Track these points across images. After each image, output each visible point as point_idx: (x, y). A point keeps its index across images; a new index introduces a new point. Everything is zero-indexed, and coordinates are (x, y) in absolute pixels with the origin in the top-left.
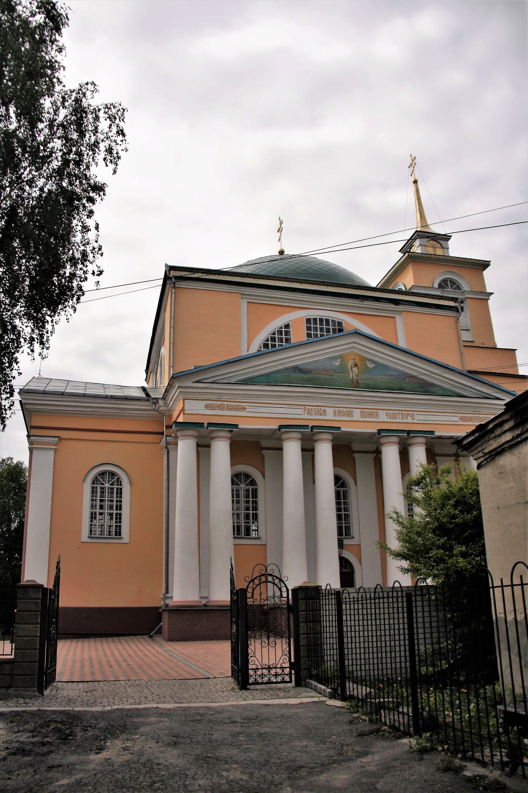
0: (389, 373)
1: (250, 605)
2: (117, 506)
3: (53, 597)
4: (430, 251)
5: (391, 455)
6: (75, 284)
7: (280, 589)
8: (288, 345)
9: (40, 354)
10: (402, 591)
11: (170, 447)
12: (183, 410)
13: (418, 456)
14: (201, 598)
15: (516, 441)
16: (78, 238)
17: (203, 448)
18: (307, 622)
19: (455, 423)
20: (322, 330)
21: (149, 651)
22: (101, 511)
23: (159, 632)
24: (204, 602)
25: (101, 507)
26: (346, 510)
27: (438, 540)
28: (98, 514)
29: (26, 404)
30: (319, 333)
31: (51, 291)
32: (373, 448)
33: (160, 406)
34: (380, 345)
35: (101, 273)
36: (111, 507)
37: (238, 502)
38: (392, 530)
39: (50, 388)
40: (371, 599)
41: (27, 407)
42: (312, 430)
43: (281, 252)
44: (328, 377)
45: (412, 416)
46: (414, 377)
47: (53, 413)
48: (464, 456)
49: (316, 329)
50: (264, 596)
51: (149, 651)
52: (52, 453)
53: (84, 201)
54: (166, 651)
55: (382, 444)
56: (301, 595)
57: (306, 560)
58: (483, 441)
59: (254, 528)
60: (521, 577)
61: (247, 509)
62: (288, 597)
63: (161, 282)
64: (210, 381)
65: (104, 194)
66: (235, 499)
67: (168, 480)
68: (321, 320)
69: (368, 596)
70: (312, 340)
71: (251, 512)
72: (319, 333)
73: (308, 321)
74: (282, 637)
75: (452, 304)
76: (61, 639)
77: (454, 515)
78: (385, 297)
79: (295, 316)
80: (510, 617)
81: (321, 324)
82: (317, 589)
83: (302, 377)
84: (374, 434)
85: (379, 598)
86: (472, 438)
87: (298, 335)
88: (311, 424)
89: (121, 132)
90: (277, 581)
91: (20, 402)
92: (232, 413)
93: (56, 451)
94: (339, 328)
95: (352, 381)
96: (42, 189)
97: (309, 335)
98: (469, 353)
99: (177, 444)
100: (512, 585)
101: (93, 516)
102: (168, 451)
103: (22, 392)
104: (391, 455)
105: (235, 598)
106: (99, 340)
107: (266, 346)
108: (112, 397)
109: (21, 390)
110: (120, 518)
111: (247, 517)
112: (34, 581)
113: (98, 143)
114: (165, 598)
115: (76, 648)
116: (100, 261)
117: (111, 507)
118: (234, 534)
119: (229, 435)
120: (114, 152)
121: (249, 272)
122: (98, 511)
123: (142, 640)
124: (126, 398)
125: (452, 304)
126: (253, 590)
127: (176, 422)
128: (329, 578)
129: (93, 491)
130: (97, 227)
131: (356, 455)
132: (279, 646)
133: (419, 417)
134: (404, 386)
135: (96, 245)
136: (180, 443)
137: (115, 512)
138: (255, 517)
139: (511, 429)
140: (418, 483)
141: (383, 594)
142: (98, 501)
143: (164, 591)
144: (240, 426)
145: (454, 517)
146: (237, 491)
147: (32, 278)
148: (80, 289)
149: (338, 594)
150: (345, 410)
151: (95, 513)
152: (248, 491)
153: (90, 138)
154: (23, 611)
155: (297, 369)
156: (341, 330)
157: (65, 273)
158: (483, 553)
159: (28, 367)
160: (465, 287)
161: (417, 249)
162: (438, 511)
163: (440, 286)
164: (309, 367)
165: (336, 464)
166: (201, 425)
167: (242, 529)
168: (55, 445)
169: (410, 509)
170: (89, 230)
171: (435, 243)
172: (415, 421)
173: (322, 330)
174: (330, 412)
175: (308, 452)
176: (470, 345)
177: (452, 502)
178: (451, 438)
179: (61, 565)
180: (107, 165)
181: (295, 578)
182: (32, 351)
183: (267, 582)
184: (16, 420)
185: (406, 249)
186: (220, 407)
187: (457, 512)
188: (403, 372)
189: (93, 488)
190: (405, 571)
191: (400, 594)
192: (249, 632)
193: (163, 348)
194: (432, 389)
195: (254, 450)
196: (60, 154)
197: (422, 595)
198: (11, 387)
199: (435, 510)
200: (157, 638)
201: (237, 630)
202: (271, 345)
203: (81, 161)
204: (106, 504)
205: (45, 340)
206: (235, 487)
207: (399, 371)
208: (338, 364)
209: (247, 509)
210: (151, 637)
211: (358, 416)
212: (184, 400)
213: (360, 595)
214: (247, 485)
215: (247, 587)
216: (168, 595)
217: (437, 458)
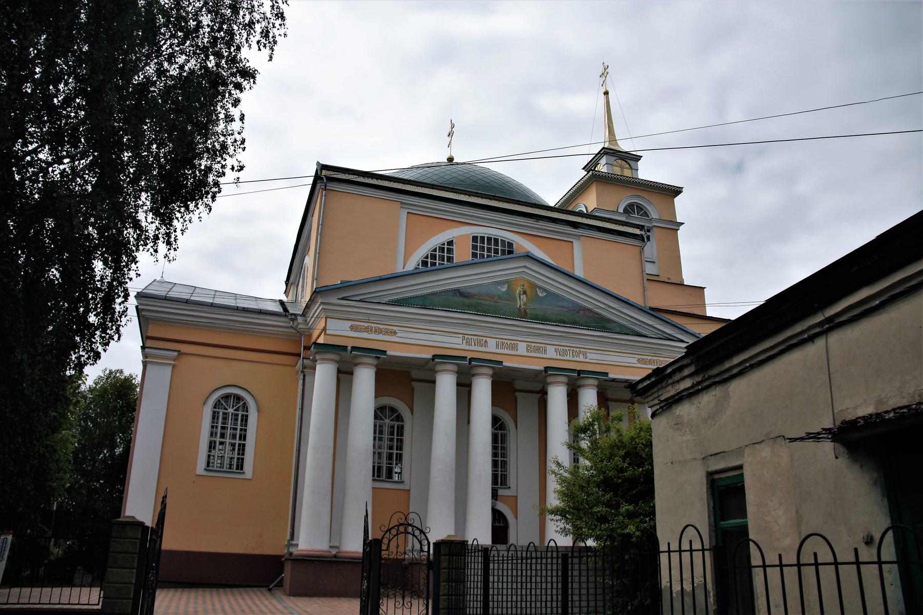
0: (561, 304)
1: (385, 559)
2: (240, 436)
3: (154, 537)
4: (617, 171)
5: (557, 396)
6: (211, 178)
7: (420, 542)
8: (450, 265)
9: (166, 256)
10: (557, 552)
11: (308, 371)
12: (324, 329)
13: (589, 399)
14: (331, 547)
15: (696, 388)
16: (221, 127)
17: (344, 375)
18: (449, 582)
19: (630, 364)
20: (488, 250)
21: (266, 606)
22: (222, 440)
23: (280, 585)
24: (334, 552)
25: (223, 436)
26: (503, 455)
27: (603, 496)
28: (218, 443)
29: (143, 310)
30: (486, 253)
31: (184, 186)
32: (538, 387)
33: (299, 324)
34: (554, 272)
35: (241, 168)
36: (234, 436)
37: (380, 439)
38: (553, 485)
39: (172, 294)
40: (522, 559)
41: (143, 313)
42: (470, 363)
43: (450, 159)
44: (492, 303)
45: (585, 355)
46: (589, 310)
47: (174, 321)
48: (639, 403)
49: (482, 249)
50: (401, 549)
51: (266, 606)
52: (170, 368)
53: (231, 87)
54: (286, 608)
55: (549, 384)
56: (444, 550)
57: (452, 509)
58: (660, 386)
59: (397, 470)
60: (691, 542)
61: (391, 448)
62: (429, 551)
63: (311, 180)
64: (358, 298)
65: (254, 82)
66: (377, 435)
67: (302, 409)
68: (489, 239)
69: (519, 555)
70: (476, 260)
71: (395, 451)
72: (486, 253)
73: (475, 239)
74: (419, 597)
75: (637, 232)
76: (163, 587)
77: (622, 468)
78: (564, 218)
79: (461, 233)
80: (676, 588)
81: (489, 243)
82: (464, 543)
83: (463, 301)
84: (540, 371)
85: (532, 558)
86: (648, 382)
87: (462, 253)
88: (469, 355)
89: (281, 16)
90: (417, 533)
91: (137, 307)
92: (381, 337)
93: (174, 366)
94: (509, 249)
95: (520, 310)
96: (181, 67)
97: (474, 255)
98: (653, 289)
99: (315, 369)
100: (680, 551)
101: (212, 446)
102: (304, 376)
103: (139, 296)
104: (557, 396)
105: (368, 550)
106: (233, 244)
107: (425, 263)
108: (245, 310)
109: (138, 293)
110: (244, 450)
111: (390, 457)
112: (133, 517)
113: (254, 24)
114: (290, 545)
115: (180, 599)
116: (241, 156)
117: (234, 436)
118: (373, 476)
119: (375, 362)
120: (271, 35)
121: (412, 179)
122: (218, 439)
123: (259, 593)
124: (260, 312)
125: (637, 232)
126: (390, 541)
127: (315, 343)
128: (479, 532)
129: (215, 416)
130: (242, 118)
131: (518, 394)
132: (415, 608)
133: (592, 357)
134: (577, 319)
135: (238, 137)
136: (318, 367)
137: (237, 442)
138: (400, 458)
139: (690, 375)
140: (584, 430)
141: (540, 553)
142: (219, 428)
143: (288, 537)
144: (389, 353)
145: (622, 470)
146: (381, 426)
147: (161, 167)
148: (217, 184)
149: (485, 551)
150: (509, 342)
151: (215, 442)
152: (393, 427)
153: (244, 16)
154: (119, 553)
155: (458, 292)
156: (510, 252)
157: (200, 165)
158: (652, 514)
159: (148, 269)
160: (654, 214)
161: (602, 168)
162: (605, 463)
163: (626, 211)
164: (471, 291)
165: (495, 402)
166: (344, 348)
167: (383, 471)
168: (174, 360)
169: (576, 460)
170: (233, 120)
171: (624, 163)
172: (587, 360)
173: (488, 250)
174: (492, 343)
175: (464, 389)
176: (654, 279)
177: (622, 453)
178: (626, 381)
179: (168, 501)
180: (260, 50)
181: (440, 528)
182: (156, 251)
183: (406, 533)
184: (131, 329)
185: (590, 167)
186: (367, 330)
187: (626, 465)
188: (577, 304)
189: (214, 412)
190: (564, 532)
191: (555, 555)
192: (382, 590)
193: (307, 257)
194: (609, 325)
195: (404, 381)
196: (208, 30)
197: (580, 557)
198: (126, 290)
199: (602, 461)
200: (277, 592)
201: (368, 587)
202: (429, 264)
203: (232, 39)
204: (229, 432)
205: (172, 239)
206: (378, 422)
207: (573, 302)
208: (504, 289)
209: (391, 448)
210: (270, 590)
211: (524, 350)
212: (326, 318)
213: (510, 553)
214: (392, 420)
215: (383, 538)
216: (293, 542)
217: (610, 403)
